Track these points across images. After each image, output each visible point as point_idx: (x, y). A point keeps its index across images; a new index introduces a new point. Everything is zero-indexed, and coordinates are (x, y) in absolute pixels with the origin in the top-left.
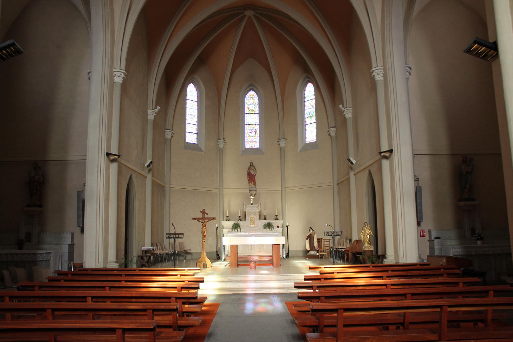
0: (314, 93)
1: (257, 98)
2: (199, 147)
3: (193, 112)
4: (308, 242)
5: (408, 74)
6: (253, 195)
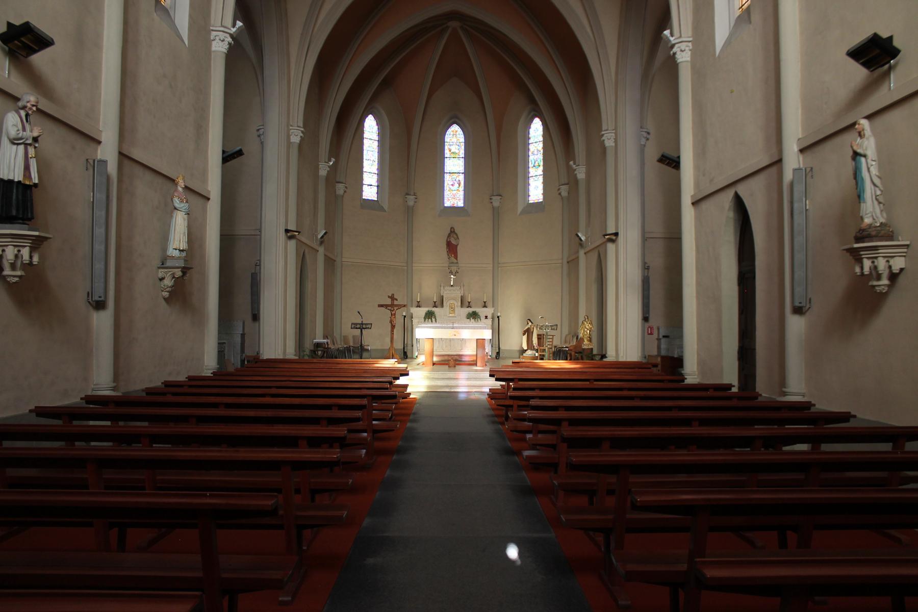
1: (463, 136)
4: (525, 338)
6: (454, 273)
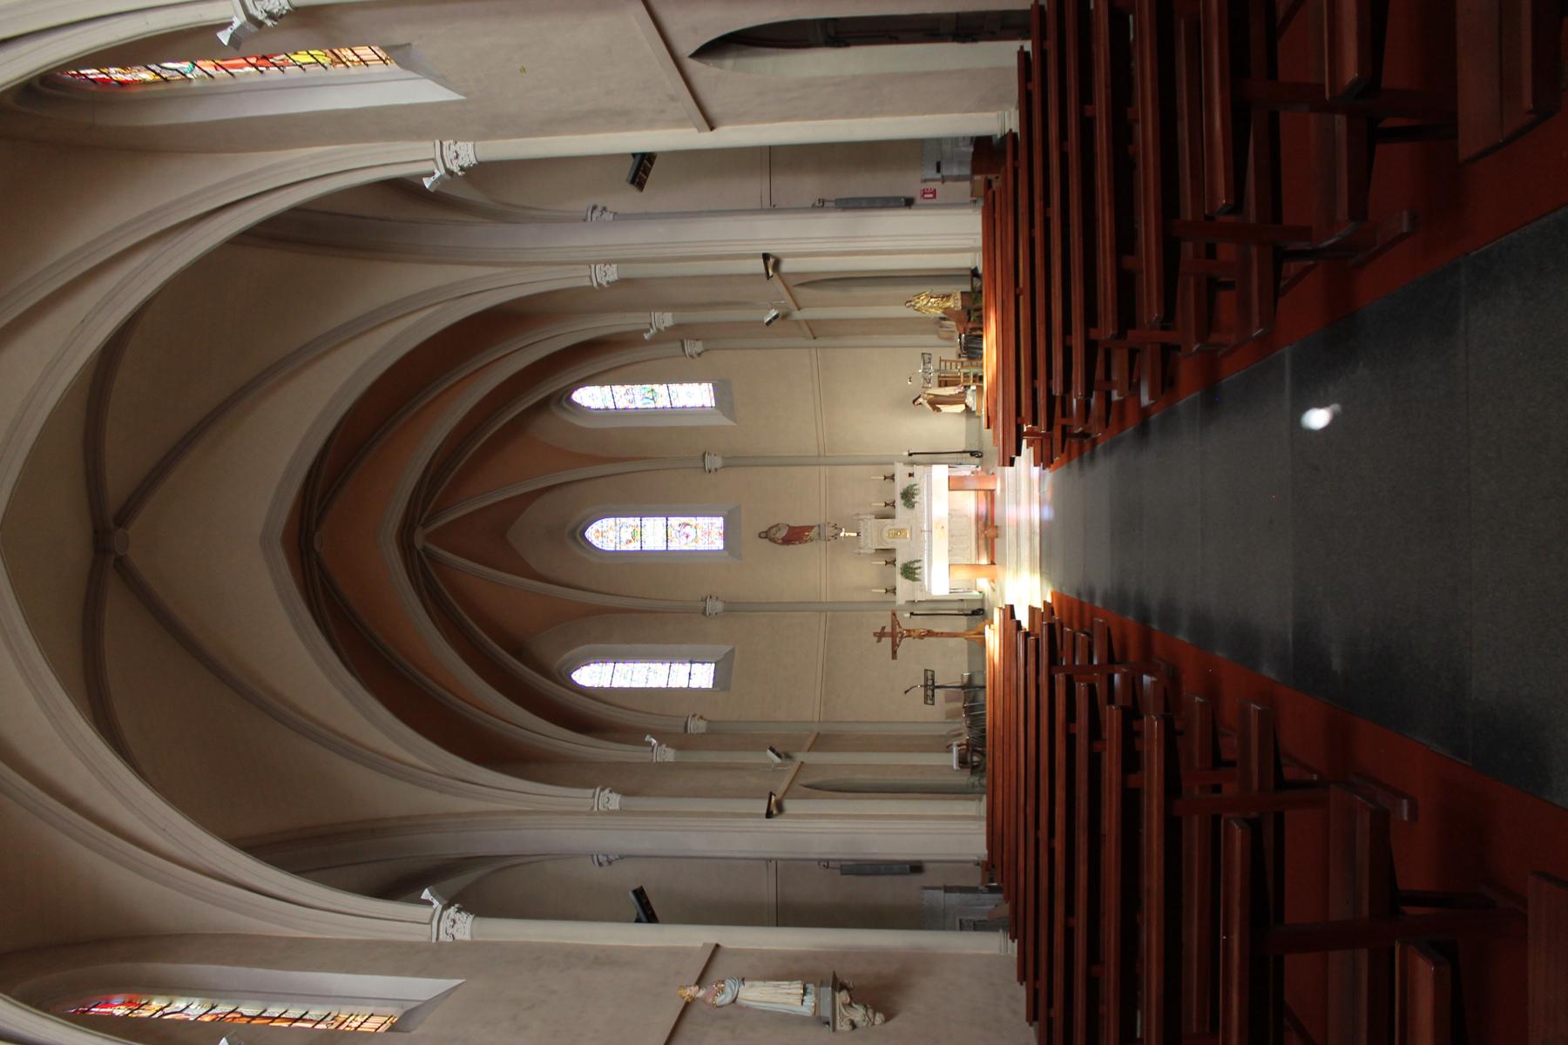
0: (597, 388)
1: (599, 522)
2: (722, 659)
3: (640, 671)
5: (605, 215)
